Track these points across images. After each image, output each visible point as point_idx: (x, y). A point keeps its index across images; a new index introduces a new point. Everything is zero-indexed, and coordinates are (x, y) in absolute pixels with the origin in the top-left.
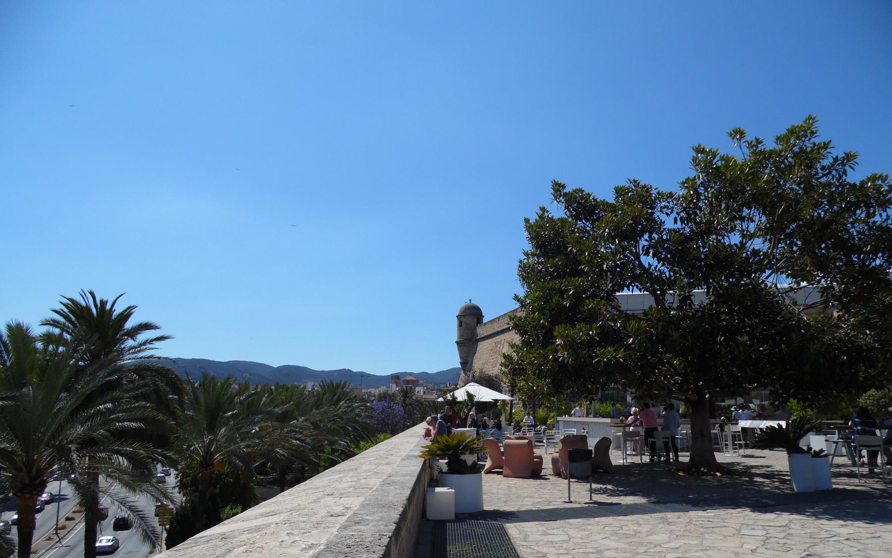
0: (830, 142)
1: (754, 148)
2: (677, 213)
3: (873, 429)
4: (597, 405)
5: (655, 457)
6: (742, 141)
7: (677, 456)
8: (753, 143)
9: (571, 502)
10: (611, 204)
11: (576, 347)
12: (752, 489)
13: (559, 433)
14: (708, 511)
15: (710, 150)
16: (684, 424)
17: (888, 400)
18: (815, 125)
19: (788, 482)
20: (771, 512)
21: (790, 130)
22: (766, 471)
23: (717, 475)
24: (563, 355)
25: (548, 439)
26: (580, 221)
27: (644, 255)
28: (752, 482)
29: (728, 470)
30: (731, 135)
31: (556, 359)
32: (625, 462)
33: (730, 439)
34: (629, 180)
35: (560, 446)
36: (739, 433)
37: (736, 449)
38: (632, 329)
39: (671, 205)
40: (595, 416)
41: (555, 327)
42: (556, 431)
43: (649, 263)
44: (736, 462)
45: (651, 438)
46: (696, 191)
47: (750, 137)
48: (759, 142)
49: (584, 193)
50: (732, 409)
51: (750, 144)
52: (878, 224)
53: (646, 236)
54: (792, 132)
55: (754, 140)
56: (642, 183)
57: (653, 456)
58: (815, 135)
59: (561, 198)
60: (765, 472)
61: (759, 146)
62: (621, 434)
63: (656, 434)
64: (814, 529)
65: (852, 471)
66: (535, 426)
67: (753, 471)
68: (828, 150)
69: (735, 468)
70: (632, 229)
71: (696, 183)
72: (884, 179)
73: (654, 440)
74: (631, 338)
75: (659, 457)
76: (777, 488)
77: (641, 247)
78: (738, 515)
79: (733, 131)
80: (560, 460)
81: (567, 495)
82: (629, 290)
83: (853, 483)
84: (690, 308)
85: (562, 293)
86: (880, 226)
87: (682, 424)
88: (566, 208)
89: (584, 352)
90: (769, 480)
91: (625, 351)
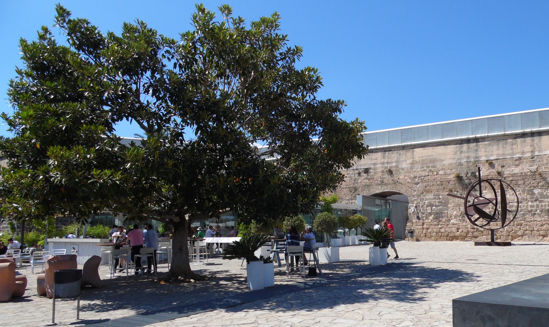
0: (286, 36)
1: (238, 25)
2: (177, 59)
3: (298, 242)
4: (88, 228)
5: (140, 270)
6: (229, 17)
7: (156, 268)
8: (237, 21)
9: (56, 324)
10: (118, 37)
11: (70, 168)
12: (221, 291)
13: (47, 253)
14: (191, 316)
15: (209, 13)
16: (163, 241)
17: (300, 222)
18: (279, 20)
19: (244, 283)
20: (241, 311)
21: (262, 19)
22: (227, 275)
23: (191, 282)
24: (56, 176)
25: (34, 260)
26: (82, 52)
27: (144, 93)
28: (218, 285)
29: (198, 276)
30: (221, 9)
31: (47, 180)
32: (112, 276)
33: (198, 251)
34: (138, 20)
35: (47, 266)
36: (204, 247)
37: (202, 259)
38: (131, 155)
39: (172, 51)
40: (85, 237)
41: (49, 147)
42: (46, 252)
43: (148, 101)
44: (203, 270)
45: (137, 254)
46: (194, 43)
47: (235, 15)
48: (241, 20)
49: (90, 25)
50: (198, 229)
51: (234, 21)
52: (308, 102)
53: (149, 73)
54: (263, 21)
55: (238, 18)
56: (149, 27)
57: (137, 270)
58: (277, 28)
59: (65, 24)
60: (226, 276)
61: (241, 24)
62: (109, 252)
63: (142, 250)
64: (276, 322)
65: (280, 271)
66: (22, 248)
67: (218, 276)
68: (285, 42)
69: (204, 274)
70: (137, 62)
71: (195, 37)
72: (315, 71)
73: (140, 256)
74: (129, 163)
75: (144, 269)
76: (238, 288)
77: (142, 84)
78: (216, 317)
79: (223, 6)
80: (46, 280)
81: (51, 317)
82: (128, 121)
83: (284, 279)
84: (182, 143)
85: (58, 116)
86: (310, 103)
87: (160, 241)
88: (69, 34)
89: (80, 173)
90: (230, 283)
91: (121, 174)
